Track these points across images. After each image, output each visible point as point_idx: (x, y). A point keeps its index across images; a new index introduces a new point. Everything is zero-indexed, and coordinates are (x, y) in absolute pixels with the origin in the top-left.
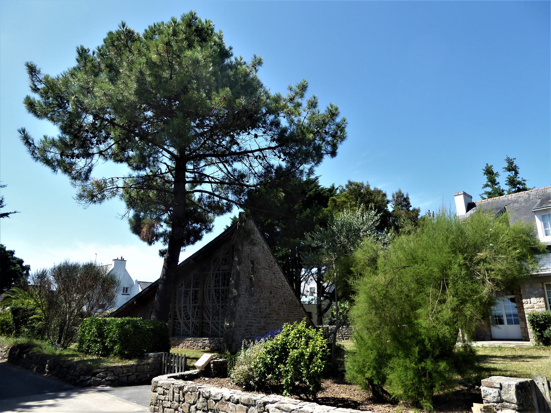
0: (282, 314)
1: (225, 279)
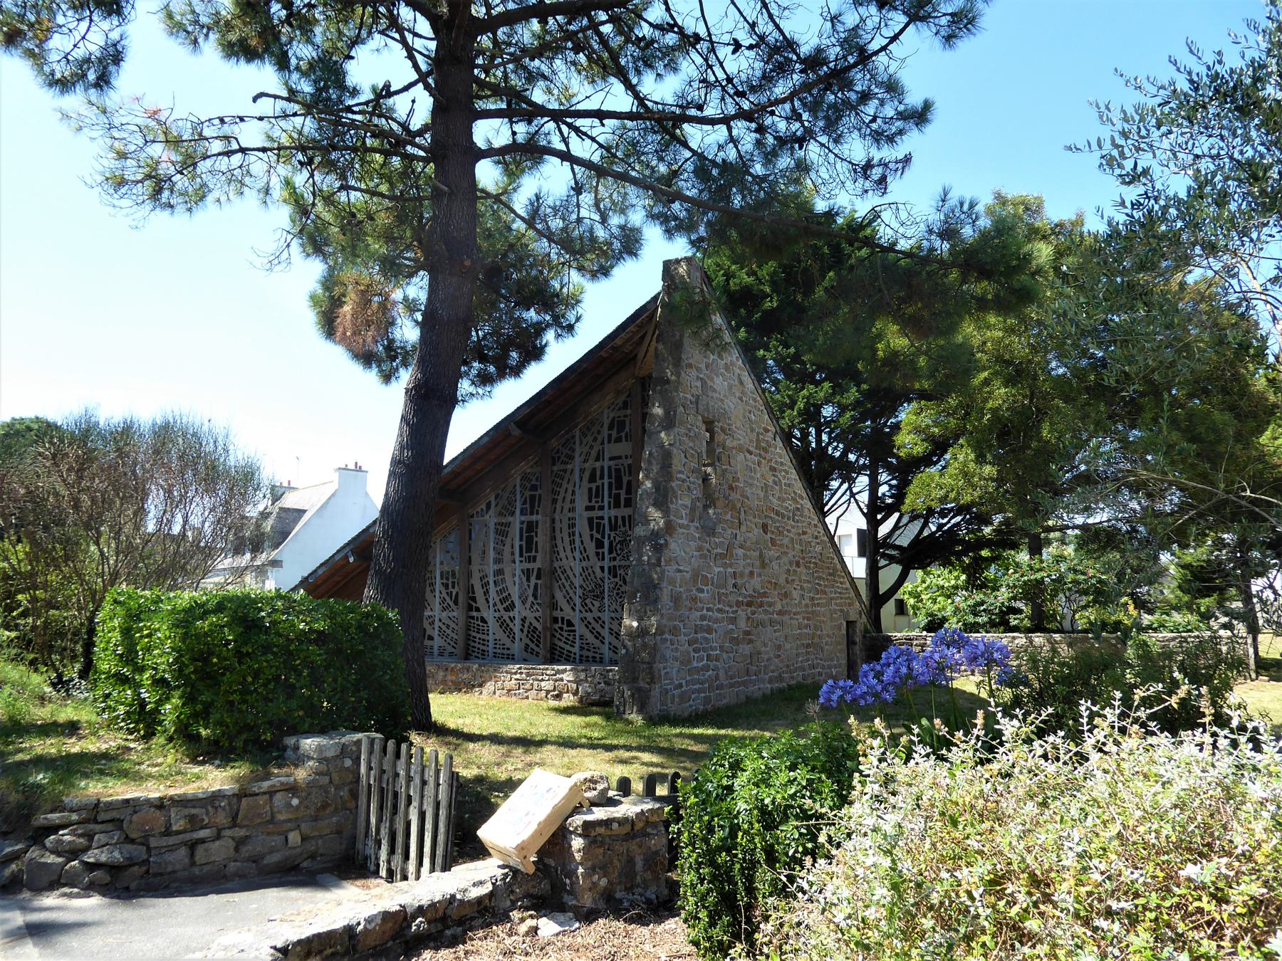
0: (795, 594)
1: (619, 487)
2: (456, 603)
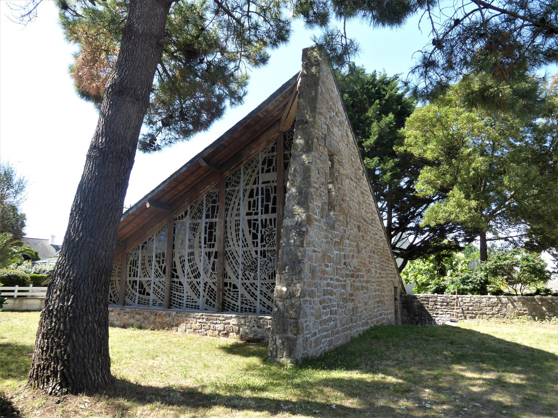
0: (373, 270)
1: (268, 200)
2: (164, 273)
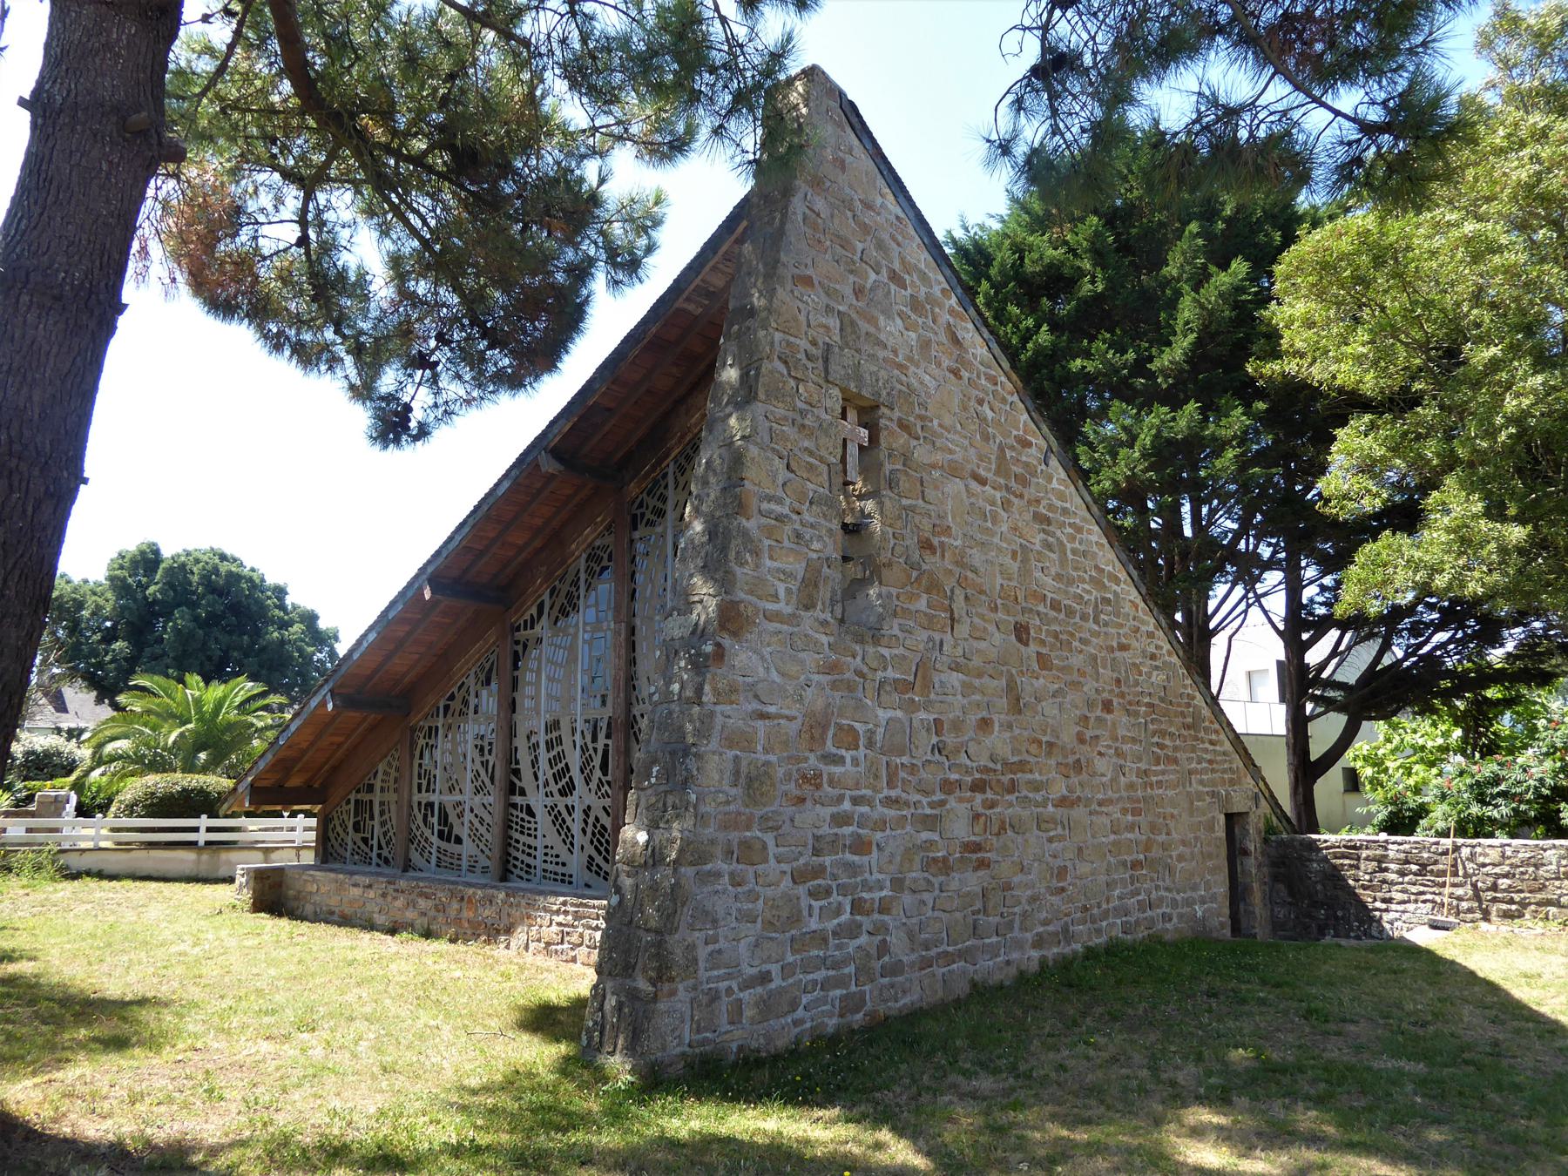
0: (1101, 765)
